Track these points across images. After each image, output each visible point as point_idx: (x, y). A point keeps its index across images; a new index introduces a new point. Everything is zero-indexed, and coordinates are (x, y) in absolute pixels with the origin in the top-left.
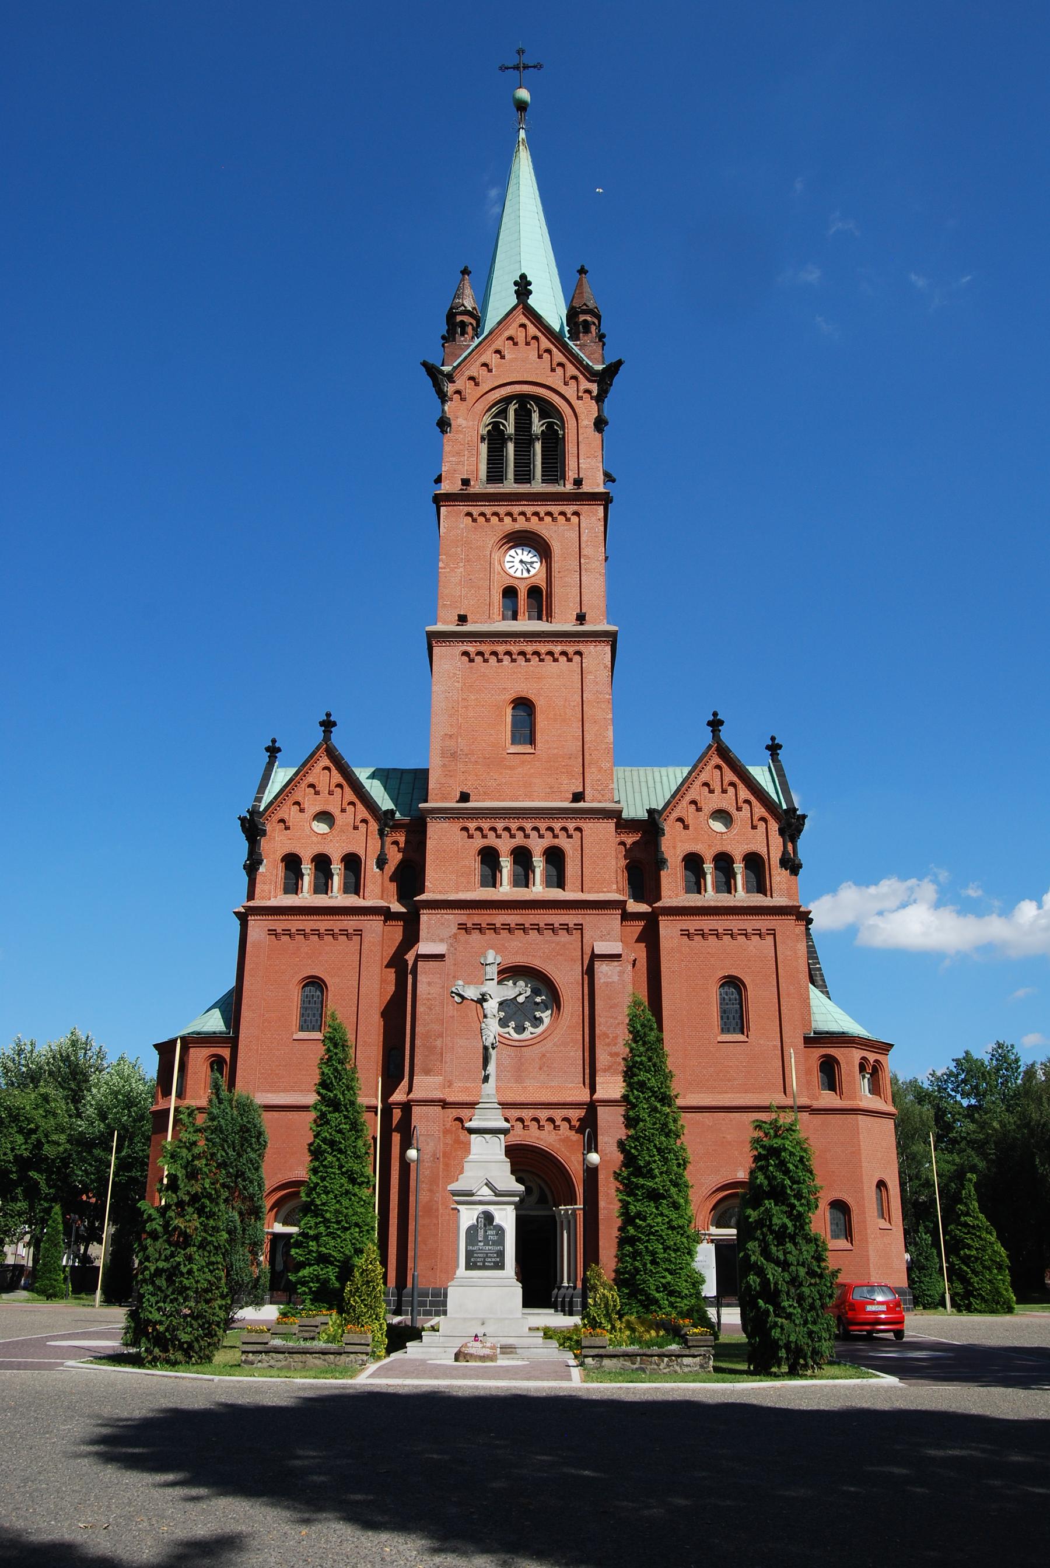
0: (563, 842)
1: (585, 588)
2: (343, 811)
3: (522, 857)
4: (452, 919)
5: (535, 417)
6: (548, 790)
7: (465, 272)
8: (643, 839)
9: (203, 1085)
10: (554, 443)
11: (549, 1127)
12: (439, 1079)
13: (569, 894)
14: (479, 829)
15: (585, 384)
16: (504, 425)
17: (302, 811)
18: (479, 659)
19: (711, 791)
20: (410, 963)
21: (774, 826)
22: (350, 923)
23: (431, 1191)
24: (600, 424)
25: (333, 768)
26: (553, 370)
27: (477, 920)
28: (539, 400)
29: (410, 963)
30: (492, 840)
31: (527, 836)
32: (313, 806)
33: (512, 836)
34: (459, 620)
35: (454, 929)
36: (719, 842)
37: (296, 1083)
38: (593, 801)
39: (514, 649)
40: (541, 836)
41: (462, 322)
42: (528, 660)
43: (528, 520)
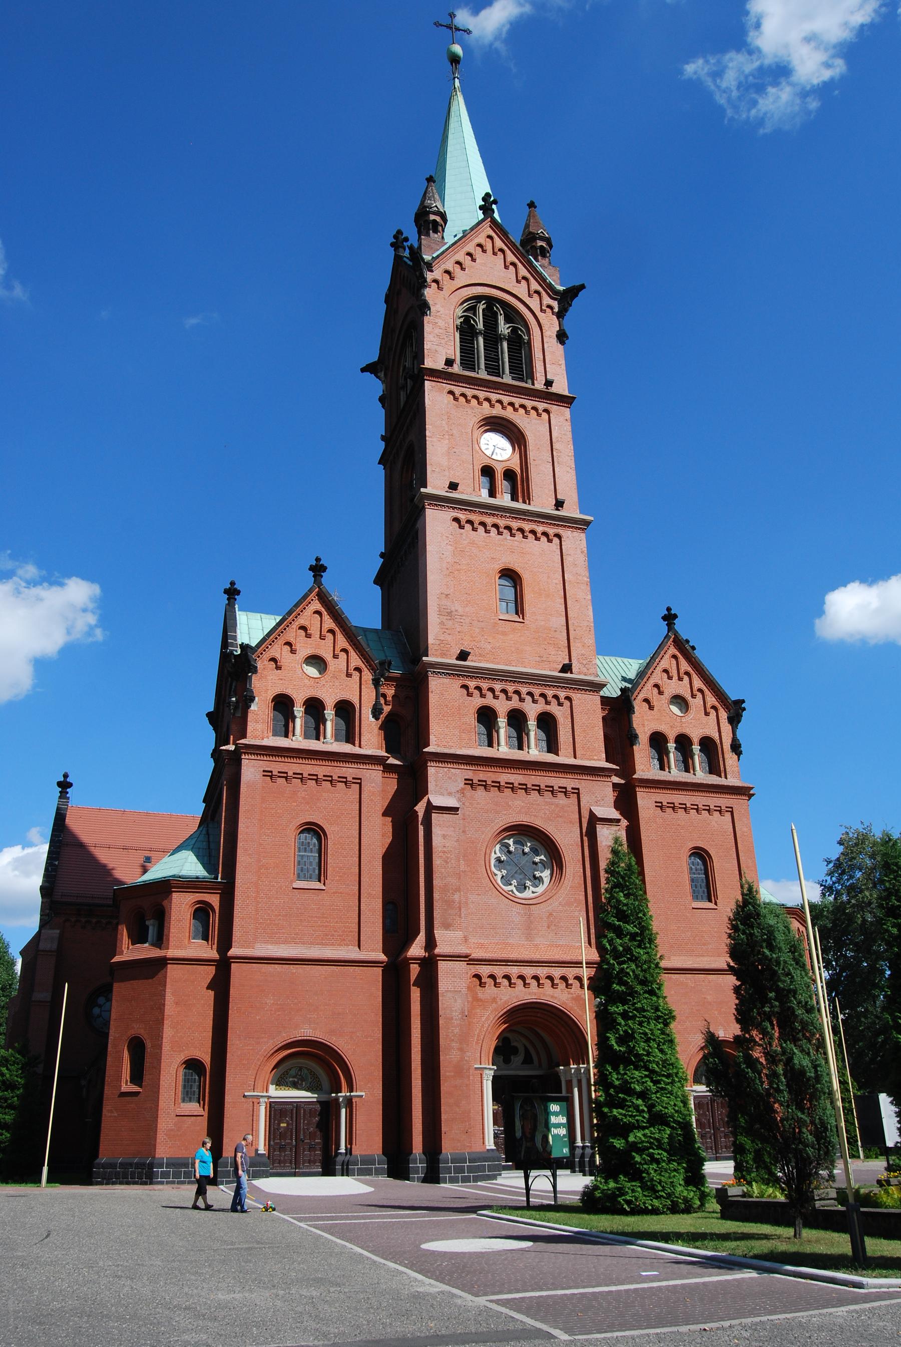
0: (554, 708)
1: (557, 477)
2: (335, 656)
3: (517, 719)
4: (460, 774)
5: (501, 319)
6: (538, 659)
7: (430, 180)
8: (618, 712)
9: (187, 935)
10: (520, 346)
11: (562, 985)
12: (459, 934)
13: (564, 758)
14: (478, 688)
15: (547, 300)
16: (474, 321)
17: (293, 651)
18: (468, 527)
19: (670, 678)
20: (421, 815)
21: (724, 715)
22: (350, 771)
23: (461, 1050)
24: (562, 337)
25: (325, 613)
27: (482, 776)
28: (505, 305)
29: (421, 815)
30: (489, 700)
31: (522, 700)
32: (305, 648)
33: (509, 699)
34: (449, 488)
35: (462, 785)
36: (679, 725)
37: (297, 934)
38: (579, 673)
39: (502, 522)
41: (435, 220)
42: (512, 535)
43: (504, 408)
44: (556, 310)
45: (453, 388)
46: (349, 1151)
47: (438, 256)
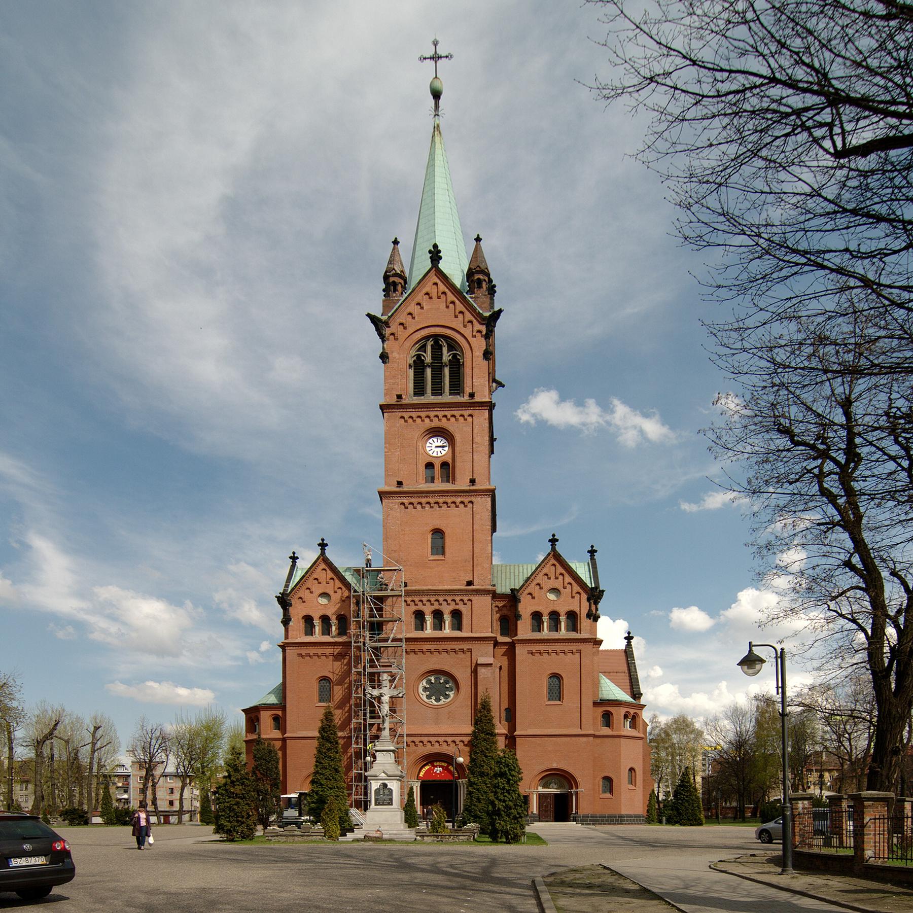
0: (461, 607)
5: (445, 350)
26: (456, 317)
28: (446, 337)
30: (420, 607)
32: (317, 589)
39: (432, 500)
40: (448, 604)
44: (484, 333)
45: (403, 414)
46: (577, 813)
47: (392, 315)
